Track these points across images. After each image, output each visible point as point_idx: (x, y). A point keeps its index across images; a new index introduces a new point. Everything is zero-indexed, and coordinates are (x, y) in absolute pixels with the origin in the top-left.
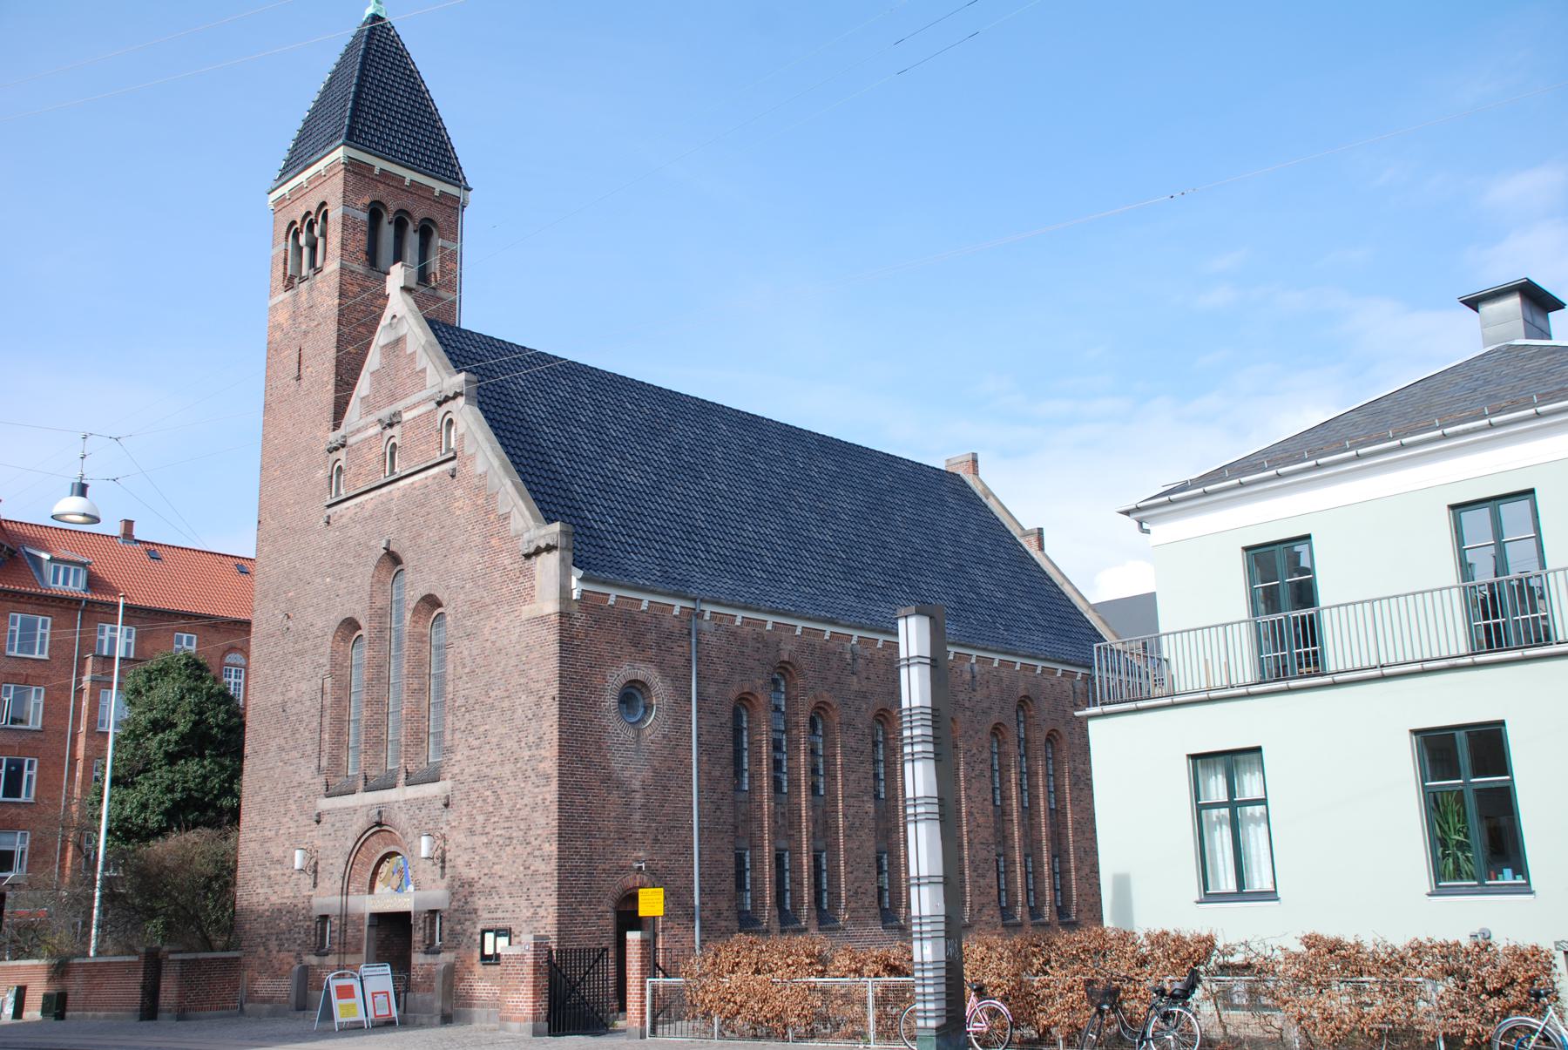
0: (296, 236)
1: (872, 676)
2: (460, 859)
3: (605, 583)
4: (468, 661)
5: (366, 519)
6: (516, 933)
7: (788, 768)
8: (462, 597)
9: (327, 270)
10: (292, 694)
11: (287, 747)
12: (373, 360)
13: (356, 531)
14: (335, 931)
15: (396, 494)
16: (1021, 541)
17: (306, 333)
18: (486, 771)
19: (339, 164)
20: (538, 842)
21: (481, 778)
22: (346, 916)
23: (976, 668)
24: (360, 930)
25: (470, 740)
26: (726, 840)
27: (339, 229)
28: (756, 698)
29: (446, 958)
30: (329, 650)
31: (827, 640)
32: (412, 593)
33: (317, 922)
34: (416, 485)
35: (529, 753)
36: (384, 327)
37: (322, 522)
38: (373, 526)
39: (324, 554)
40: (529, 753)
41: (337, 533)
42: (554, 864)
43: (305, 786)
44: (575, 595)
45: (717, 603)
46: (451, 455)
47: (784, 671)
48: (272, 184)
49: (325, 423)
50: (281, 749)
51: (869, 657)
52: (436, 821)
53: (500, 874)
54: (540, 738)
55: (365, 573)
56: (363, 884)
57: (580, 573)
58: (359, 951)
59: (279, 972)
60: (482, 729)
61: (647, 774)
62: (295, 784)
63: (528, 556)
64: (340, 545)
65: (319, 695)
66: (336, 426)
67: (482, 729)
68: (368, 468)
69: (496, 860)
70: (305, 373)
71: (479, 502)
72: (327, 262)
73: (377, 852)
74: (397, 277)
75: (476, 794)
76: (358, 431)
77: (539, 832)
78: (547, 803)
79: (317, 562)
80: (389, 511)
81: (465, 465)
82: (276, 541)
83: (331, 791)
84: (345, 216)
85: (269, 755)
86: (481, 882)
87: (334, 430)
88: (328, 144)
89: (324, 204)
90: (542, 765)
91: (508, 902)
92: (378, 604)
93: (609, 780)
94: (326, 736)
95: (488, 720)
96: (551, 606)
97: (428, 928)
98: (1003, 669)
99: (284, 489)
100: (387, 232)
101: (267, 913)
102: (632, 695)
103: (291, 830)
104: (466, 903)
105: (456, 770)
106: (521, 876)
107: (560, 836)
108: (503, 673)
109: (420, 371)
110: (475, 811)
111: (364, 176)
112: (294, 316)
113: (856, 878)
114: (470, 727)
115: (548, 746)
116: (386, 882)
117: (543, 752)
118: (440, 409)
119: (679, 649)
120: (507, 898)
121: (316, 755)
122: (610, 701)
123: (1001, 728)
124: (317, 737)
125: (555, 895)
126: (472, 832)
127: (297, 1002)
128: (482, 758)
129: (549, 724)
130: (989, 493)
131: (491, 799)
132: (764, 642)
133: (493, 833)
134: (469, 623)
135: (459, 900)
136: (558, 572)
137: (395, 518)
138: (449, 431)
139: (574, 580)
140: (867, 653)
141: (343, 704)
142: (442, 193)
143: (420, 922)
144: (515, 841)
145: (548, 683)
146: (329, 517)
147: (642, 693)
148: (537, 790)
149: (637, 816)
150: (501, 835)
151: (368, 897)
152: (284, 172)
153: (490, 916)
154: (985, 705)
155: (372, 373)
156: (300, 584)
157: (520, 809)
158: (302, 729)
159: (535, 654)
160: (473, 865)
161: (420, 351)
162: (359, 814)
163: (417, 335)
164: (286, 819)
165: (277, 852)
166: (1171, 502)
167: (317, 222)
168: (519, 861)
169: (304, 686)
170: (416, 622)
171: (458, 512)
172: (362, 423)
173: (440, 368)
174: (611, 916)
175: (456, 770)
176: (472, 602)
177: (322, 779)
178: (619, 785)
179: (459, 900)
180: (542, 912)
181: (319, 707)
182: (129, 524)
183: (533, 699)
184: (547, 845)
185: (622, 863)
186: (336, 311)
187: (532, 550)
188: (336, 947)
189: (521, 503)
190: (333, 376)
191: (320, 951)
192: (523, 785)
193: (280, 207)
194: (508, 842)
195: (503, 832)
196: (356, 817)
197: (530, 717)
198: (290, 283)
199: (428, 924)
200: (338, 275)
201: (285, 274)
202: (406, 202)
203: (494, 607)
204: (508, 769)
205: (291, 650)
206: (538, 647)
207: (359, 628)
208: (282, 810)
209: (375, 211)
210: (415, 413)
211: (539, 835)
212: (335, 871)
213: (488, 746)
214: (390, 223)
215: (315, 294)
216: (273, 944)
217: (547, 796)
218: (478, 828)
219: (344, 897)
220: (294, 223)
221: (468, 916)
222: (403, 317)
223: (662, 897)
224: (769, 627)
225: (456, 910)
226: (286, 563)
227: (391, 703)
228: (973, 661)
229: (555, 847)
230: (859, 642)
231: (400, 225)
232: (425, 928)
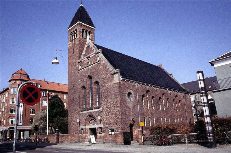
0: (72, 34)
4: (104, 90)
12: (85, 49)
18: (108, 106)
21: (107, 107)
48: (68, 28)
50: (74, 105)
58: (88, 133)
63: (112, 74)
70: (74, 52)
74: (88, 37)
76: (83, 59)
93: (127, 107)
102: (129, 94)
112: (72, 45)
116: (91, 123)
122: (127, 95)
126: (106, 116)
145: (118, 92)
149: (131, 112)
152: (69, 27)
165: (74, 120)
166: (218, 60)
169: (77, 96)
172: (84, 58)
175: (103, 106)
176: (104, 82)
182: (44, 79)
204: (112, 106)
209: (83, 30)
216: (74, 133)
231: (86, 32)
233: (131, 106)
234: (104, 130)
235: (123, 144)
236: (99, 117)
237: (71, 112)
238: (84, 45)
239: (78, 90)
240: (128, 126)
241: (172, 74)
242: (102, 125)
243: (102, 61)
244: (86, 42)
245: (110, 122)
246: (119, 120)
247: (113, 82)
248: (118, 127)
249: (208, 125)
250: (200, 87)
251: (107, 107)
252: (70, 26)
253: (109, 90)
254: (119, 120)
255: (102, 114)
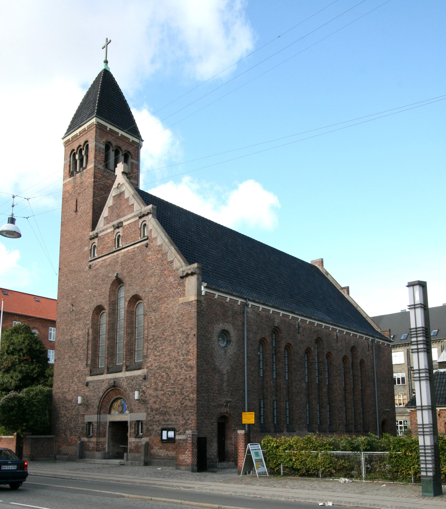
1: (305, 335)
2: (151, 400)
3: (214, 290)
5: (107, 266)
6: (177, 430)
7: (276, 368)
8: (151, 295)
9: (89, 167)
10: (75, 336)
11: (73, 356)
12: (110, 202)
13: (103, 270)
14: (95, 428)
15: (121, 255)
16: (341, 291)
17: (79, 194)
18: (163, 365)
19: (94, 125)
20: (187, 394)
22: (99, 422)
23: (338, 334)
24: (105, 428)
25: (155, 352)
26: (256, 396)
27: (94, 151)
28: (266, 340)
29: (145, 440)
30: (91, 318)
31: (290, 319)
32: (128, 294)
33: (87, 425)
34: (130, 251)
35: (183, 358)
36: (114, 189)
37: (87, 268)
38: (110, 268)
39: (88, 280)
40: (183, 358)
41: (94, 272)
42: (195, 402)
43: (81, 371)
44: (203, 293)
45: (254, 301)
46: (146, 238)
47: (276, 331)
49: (88, 229)
50: (70, 357)
51: (304, 327)
52: (140, 385)
53: (170, 406)
54: (188, 352)
55: (106, 288)
56: (107, 410)
57: (205, 284)
58: (105, 436)
59: (71, 444)
60: (161, 348)
61: (228, 368)
62: (76, 371)
63: (182, 277)
64: (95, 276)
65: (87, 336)
66: (93, 228)
67: (161, 348)
68: (108, 245)
69: (168, 401)
71: (159, 257)
72: (88, 164)
73: (112, 397)
74: (120, 168)
75: (158, 375)
76: (103, 231)
77: (188, 389)
78: (192, 378)
79: (85, 284)
80: (117, 262)
81: (152, 242)
82: (67, 276)
83: (92, 374)
84: (96, 146)
85: (65, 359)
86: (161, 409)
87: (92, 231)
88: (89, 116)
89: (87, 142)
90: (189, 363)
91: (173, 418)
92: (112, 300)
93: (215, 370)
94: (90, 352)
95: (164, 345)
96: (192, 297)
97: (136, 428)
98: (346, 335)
99: (70, 255)
100: (112, 154)
101: (65, 421)
102: (224, 333)
103: (75, 389)
104: (154, 418)
105: (149, 365)
106: (179, 407)
107: (197, 391)
108: (170, 325)
109: (131, 205)
110: (158, 381)
111: (103, 131)
112: (74, 187)
113: (299, 412)
114: (155, 347)
115: (192, 355)
117: (189, 357)
118: (140, 220)
119: (240, 319)
120: (173, 416)
121: (86, 359)
123: (346, 358)
124: (86, 352)
125: (195, 415)
126: (156, 390)
127: (79, 455)
128: (161, 360)
129: (192, 345)
130: (327, 274)
131: (165, 376)
132: (269, 318)
133: (166, 390)
134: (154, 306)
135: (151, 417)
136: (196, 284)
137: (120, 265)
138: (144, 229)
139: (203, 287)
140: (303, 326)
141: (97, 339)
142: (133, 141)
143: (133, 425)
144: (176, 393)
145: (192, 329)
146: (90, 265)
147: (226, 335)
148: (187, 372)
149: (225, 384)
150: (170, 391)
151: (108, 415)
153: (165, 423)
154: (341, 348)
155: (109, 208)
156: (78, 293)
157: (178, 380)
158: (79, 349)
159: (185, 317)
160: (157, 403)
161: (131, 197)
162: (105, 382)
163: (128, 191)
164: (73, 385)
167: (84, 150)
168: (179, 401)
169: (80, 332)
170: (130, 306)
171: (149, 261)
172: (105, 227)
173: (140, 203)
174: (216, 424)
175: (149, 365)
176: (156, 297)
177: (88, 369)
178: (219, 372)
179: (151, 417)
180: (189, 422)
181: (87, 340)
183: (184, 335)
184: (192, 395)
185: (220, 403)
186: (93, 184)
187: (184, 274)
188: (95, 434)
189: (178, 256)
190: (91, 209)
191: (88, 435)
192: (180, 371)
193: (67, 145)
194: (173, 394)
195: (171, 389)
196: (103, 384)
197: (183, 343)
198: (71, 174)
199: (136, 426)
200: (93, 169)
201: (70, 170)
202: (121, 144)
203: (166, 299)
205: (74, 318)
206: (187, 314)
207: (104, 309)
208: (71, 381)
209: (108, 146)
210: (129, 222)
211: (188, 391)
212: (95, 405)
213: (163, 355)
214: (113, 151)
215: (83, 177)
216: (68, 433)
217: (192, 375)
218: (159, 388)
219: (99, 415)
220: (74, 150)
221: (154, 423)
222: (123, 184)
223: (254, 416)
224: (271, 312)
225: (149, 421)
226: (71, 284)
227: (118, 339)
228: (337, 331)
229: (195, 396)
230: (301, 321)
231: (117, 153)
232: (135, 428)
233: (225, 368)
234: (148, 430)
235: (196, 468)
236: (136, 393)
237: (63, 377)
238: (108, 190)
239: (85, 317)
240: (214, 420)
241: (348, 287)
242: (145, 414)
243: (156, 238)
244: (114, 181)
245: (166, 407)
246: (190, 404)
247: (181, 300)
248: (186, 422)
249: (423, 432)
250: (413, 326)
251: (160, 368)
252: (72, 128)
253: (168, 322)
254: (190, 404)
255: (145, 386)
